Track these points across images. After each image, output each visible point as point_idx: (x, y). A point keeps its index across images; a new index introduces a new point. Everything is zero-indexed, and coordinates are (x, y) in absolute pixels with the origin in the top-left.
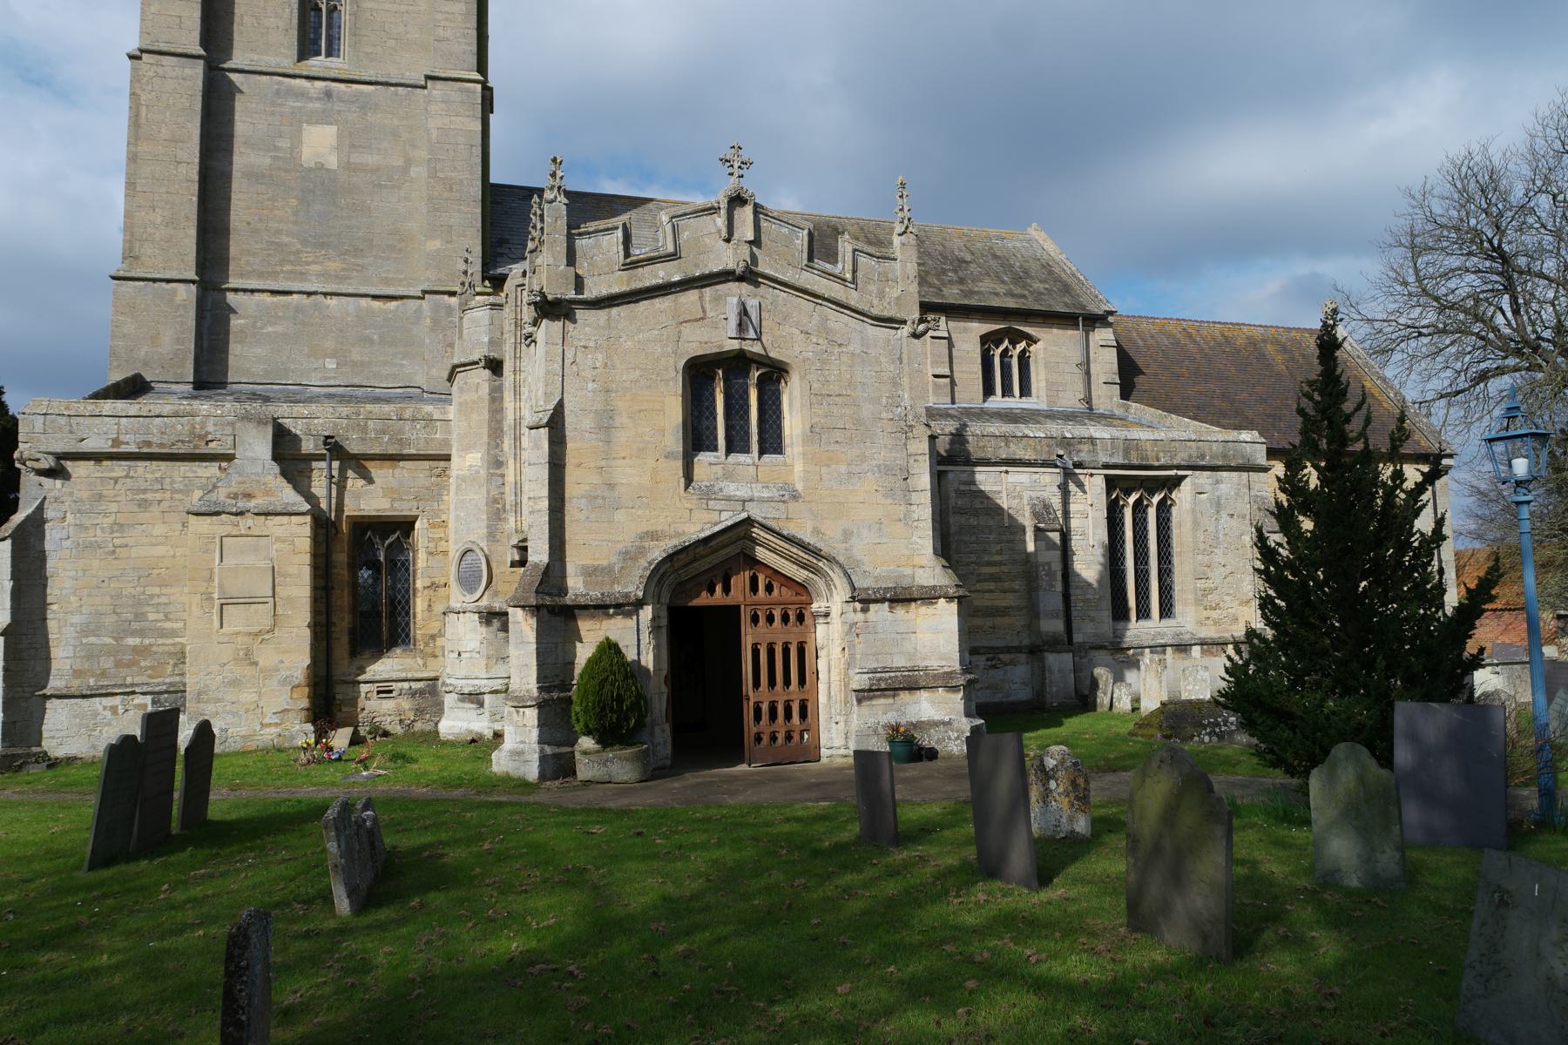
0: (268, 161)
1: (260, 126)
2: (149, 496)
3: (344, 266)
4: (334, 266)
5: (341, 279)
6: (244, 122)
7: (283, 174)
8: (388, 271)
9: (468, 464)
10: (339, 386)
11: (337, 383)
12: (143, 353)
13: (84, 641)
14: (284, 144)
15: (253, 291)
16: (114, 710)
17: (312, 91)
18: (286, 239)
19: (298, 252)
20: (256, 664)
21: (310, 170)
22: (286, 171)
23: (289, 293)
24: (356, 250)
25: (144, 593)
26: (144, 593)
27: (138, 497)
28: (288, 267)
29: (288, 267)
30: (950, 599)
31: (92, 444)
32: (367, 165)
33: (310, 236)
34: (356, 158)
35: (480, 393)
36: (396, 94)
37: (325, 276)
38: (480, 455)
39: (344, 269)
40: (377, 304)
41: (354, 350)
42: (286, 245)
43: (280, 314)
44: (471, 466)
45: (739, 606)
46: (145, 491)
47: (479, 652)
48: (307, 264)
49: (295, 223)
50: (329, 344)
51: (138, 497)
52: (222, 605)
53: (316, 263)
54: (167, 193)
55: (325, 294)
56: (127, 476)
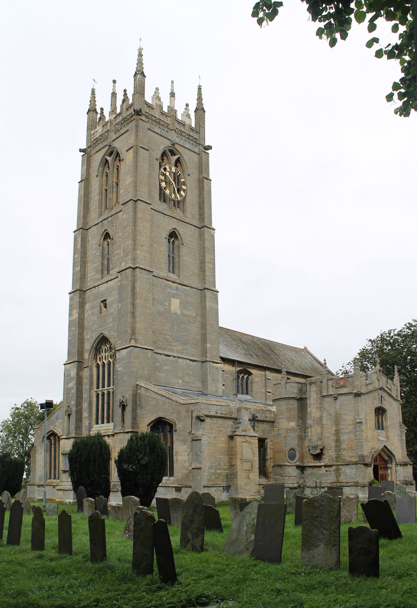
0: (163, 309)
1: (161, 297)
2: (220, 429)
3: (182, 348)
4: (180, 348)
5: (182, 353)
6: (157, 294)
7: (167, 314)
8: (193, 352)
9: (290, 425)
10: (183, 389)
11: (182, 388)
12: (140, 374)
13: (210, 471)
14: (167, 304)
15: (161, 354)
16: (216, 491)
17: (173, 286)
18: (168, 337)
19: (171, 342)
20: (249, 479)
21: (173, 314)
22: (167, 313)
23: (169, 356)
24: (185, 343)
25: (220, 458)
26: (220, 458)
27: (219, 429)
28: (169, 347)
29: (169, 347)
30: (411, 465)
31: (213, 413)
32: (187, 315)
33: (174, 337)
34: (185, 312)
35: (294, 406)
36: (193, 290)
37: (178, 352)
38: (295, 423)
39: (182, 350)
40: (191, 362)
41: (186, 377)
42: (168, 339)
43: (168, 363)
44: (292, 426)
45: (378, 465)
46: (220, 427)
47: (296, 477)
48: (174, 346)
49: (170, 332)
50: (180, 375)
51: (219, 429)
52: (251, 461)
53: (176, 346)
54: (145, 318)
55: (178, 357)
56: (216, 423)
